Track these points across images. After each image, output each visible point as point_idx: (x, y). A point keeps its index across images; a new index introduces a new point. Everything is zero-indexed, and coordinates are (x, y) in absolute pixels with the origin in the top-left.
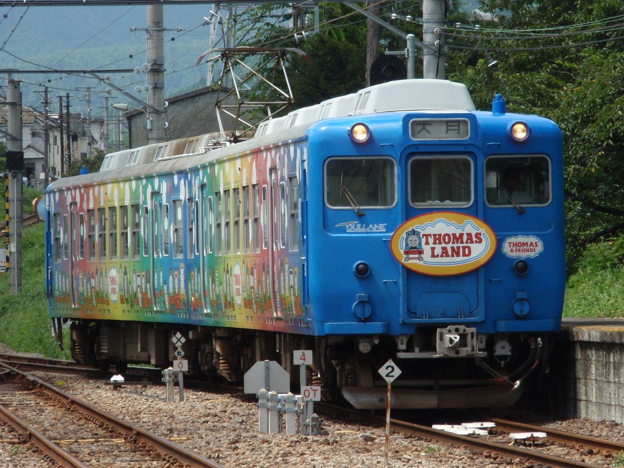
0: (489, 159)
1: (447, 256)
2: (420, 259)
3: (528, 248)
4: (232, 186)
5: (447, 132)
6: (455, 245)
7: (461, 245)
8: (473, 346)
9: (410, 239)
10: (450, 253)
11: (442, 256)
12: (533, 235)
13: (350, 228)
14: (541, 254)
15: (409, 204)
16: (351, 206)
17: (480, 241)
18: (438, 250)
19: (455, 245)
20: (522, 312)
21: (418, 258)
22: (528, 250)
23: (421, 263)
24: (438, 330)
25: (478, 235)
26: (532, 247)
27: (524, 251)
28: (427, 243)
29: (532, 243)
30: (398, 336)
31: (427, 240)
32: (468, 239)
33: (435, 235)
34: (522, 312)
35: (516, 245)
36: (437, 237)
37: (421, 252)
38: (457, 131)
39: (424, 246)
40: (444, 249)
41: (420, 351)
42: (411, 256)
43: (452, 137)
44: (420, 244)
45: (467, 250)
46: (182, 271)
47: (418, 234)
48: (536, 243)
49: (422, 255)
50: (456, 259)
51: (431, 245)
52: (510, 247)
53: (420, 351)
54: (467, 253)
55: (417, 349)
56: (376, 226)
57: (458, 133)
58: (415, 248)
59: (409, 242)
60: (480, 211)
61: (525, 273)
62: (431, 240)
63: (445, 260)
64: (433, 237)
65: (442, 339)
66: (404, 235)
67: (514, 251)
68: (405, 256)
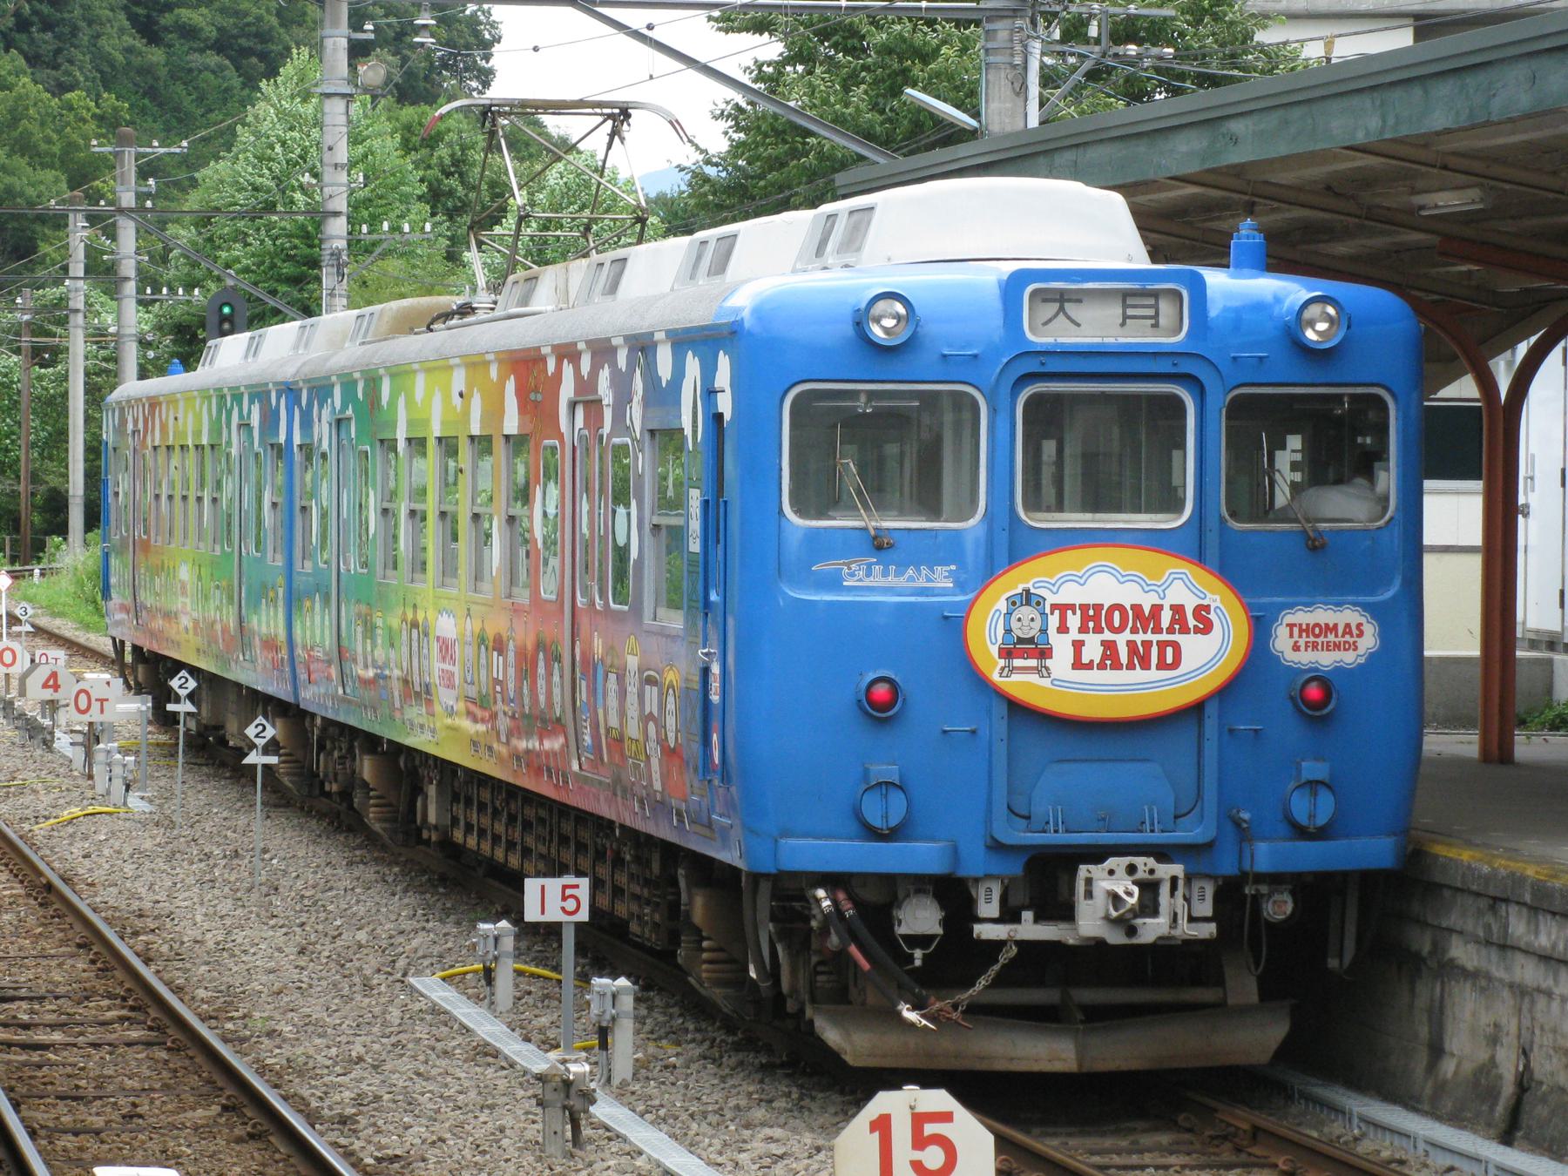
0: (1236, 396)
1: (1117, 666)
2: (1042, 671)
3: (1337, 640)
4: (436, 430)
5: (1123, 324)
6: (1139, 638)
7: (1155, 638)
8: (1175, 915)
9: (1015, 616)
10: (1124, 659)
11: (1102, 666)
12: (1355, 604)
13: (852, 575)
14: (1372, 657)
15: (1020, 520)
16: (860, 517)
17: (1206, 627)
18: (1092, 651)
19: (1139, 638)
20: (1312, 816)
21: (1037, 670)
22: (1337, 646)
23: (1046, 682)
24: (1083, 871)
25: (1201, 611)
26: (1348, 638)
27: (1328, 647)
28: (1063, 629)
29: (1348, 626)
30: (977, 880)
31: (1063, 619)
32: (1173, 621)
33: (1084, 608)
34: (1312, 816)
35: (1307, 630)
36: (1091, 612)
37: (1045, 653)
38: (1153, 321)
39: (1055, 639)
40: (1109, 646)
41: (1037, 920)
42: (1017, 662)
43: (1139, 336)
44: (1044, 631)
45: (1169, 650)
46: (281, 591)
47: (1040, 601)
48: (1359, 626)
49: (1049, 662)
50: (1139, 675)
51: (1074, 634)
52: (1291, 635)
53: (1037, 920)
54: (1169, 660)
55: (1028, 915)
56: (924, 570)
57: (1153, 326)
58: (1031, 640)
59: (1015, 625)
60: (1212, 539)
61: (1325, 711)
62: (1074, 621)
63: (1109, 676)
64: (1078, 612)
65: (1089, 894)
66: (1002, 605)
67: (1303, 648)
68: (1002, 662)
